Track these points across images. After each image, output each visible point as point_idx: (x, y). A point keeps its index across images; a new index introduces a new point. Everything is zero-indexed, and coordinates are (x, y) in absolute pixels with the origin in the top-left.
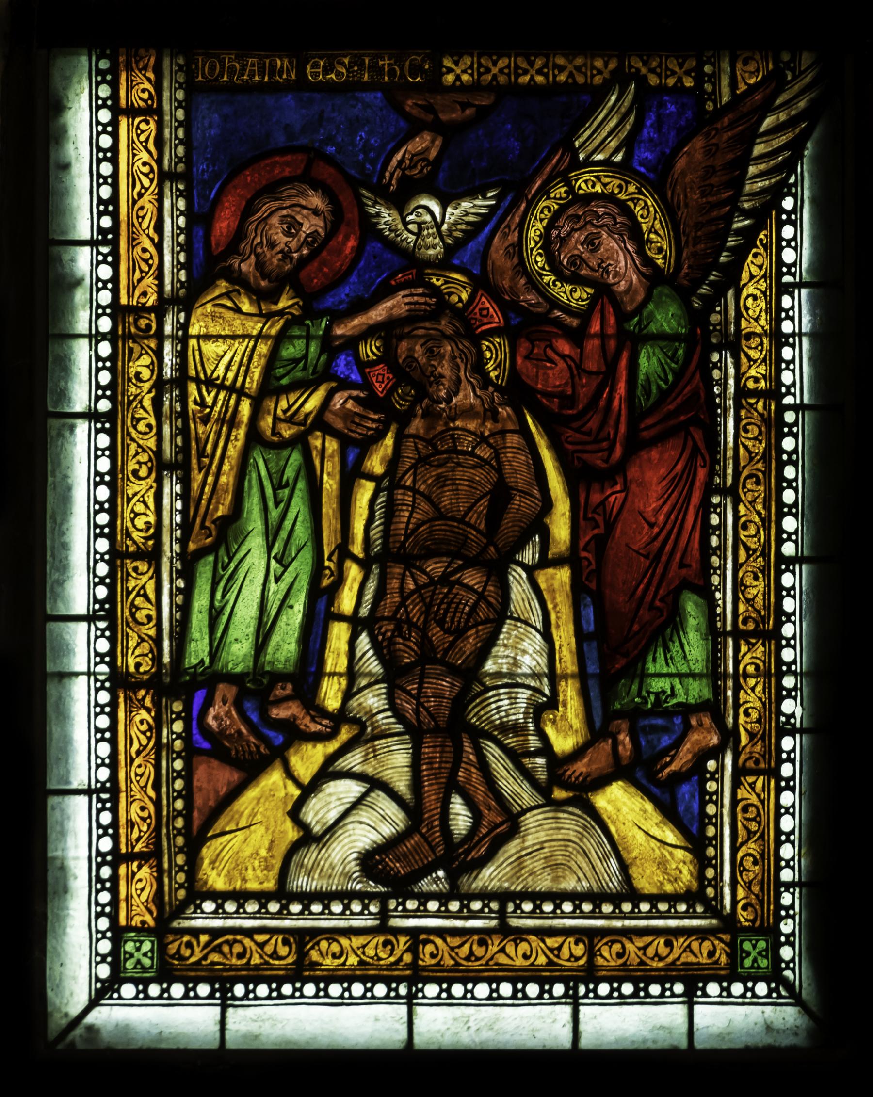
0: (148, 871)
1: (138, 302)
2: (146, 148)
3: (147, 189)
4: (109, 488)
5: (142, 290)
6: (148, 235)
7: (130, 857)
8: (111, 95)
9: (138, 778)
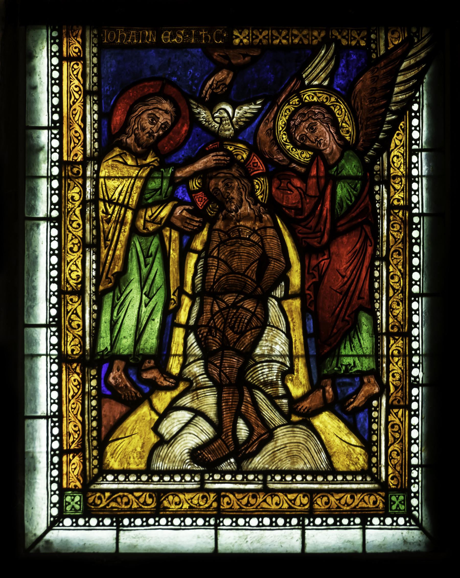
0: (78, 459)
1: (73, 159)
2: (77, 78)
3: (77, 100)
4: (57, 257)
5: (75, 153)
6: (78, 124)
7: (68, 452)
8: (58, 50)
9: (73, 410)
